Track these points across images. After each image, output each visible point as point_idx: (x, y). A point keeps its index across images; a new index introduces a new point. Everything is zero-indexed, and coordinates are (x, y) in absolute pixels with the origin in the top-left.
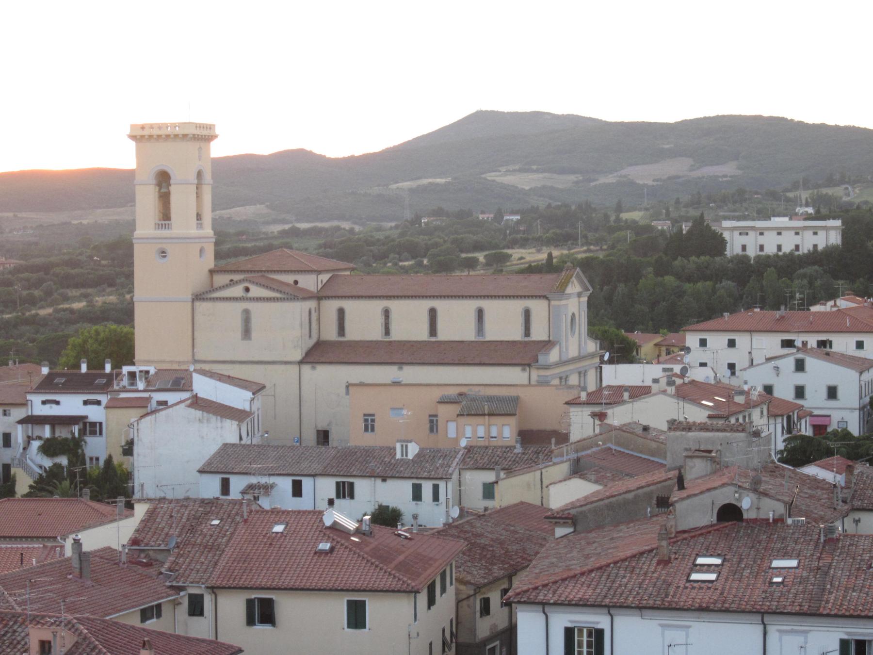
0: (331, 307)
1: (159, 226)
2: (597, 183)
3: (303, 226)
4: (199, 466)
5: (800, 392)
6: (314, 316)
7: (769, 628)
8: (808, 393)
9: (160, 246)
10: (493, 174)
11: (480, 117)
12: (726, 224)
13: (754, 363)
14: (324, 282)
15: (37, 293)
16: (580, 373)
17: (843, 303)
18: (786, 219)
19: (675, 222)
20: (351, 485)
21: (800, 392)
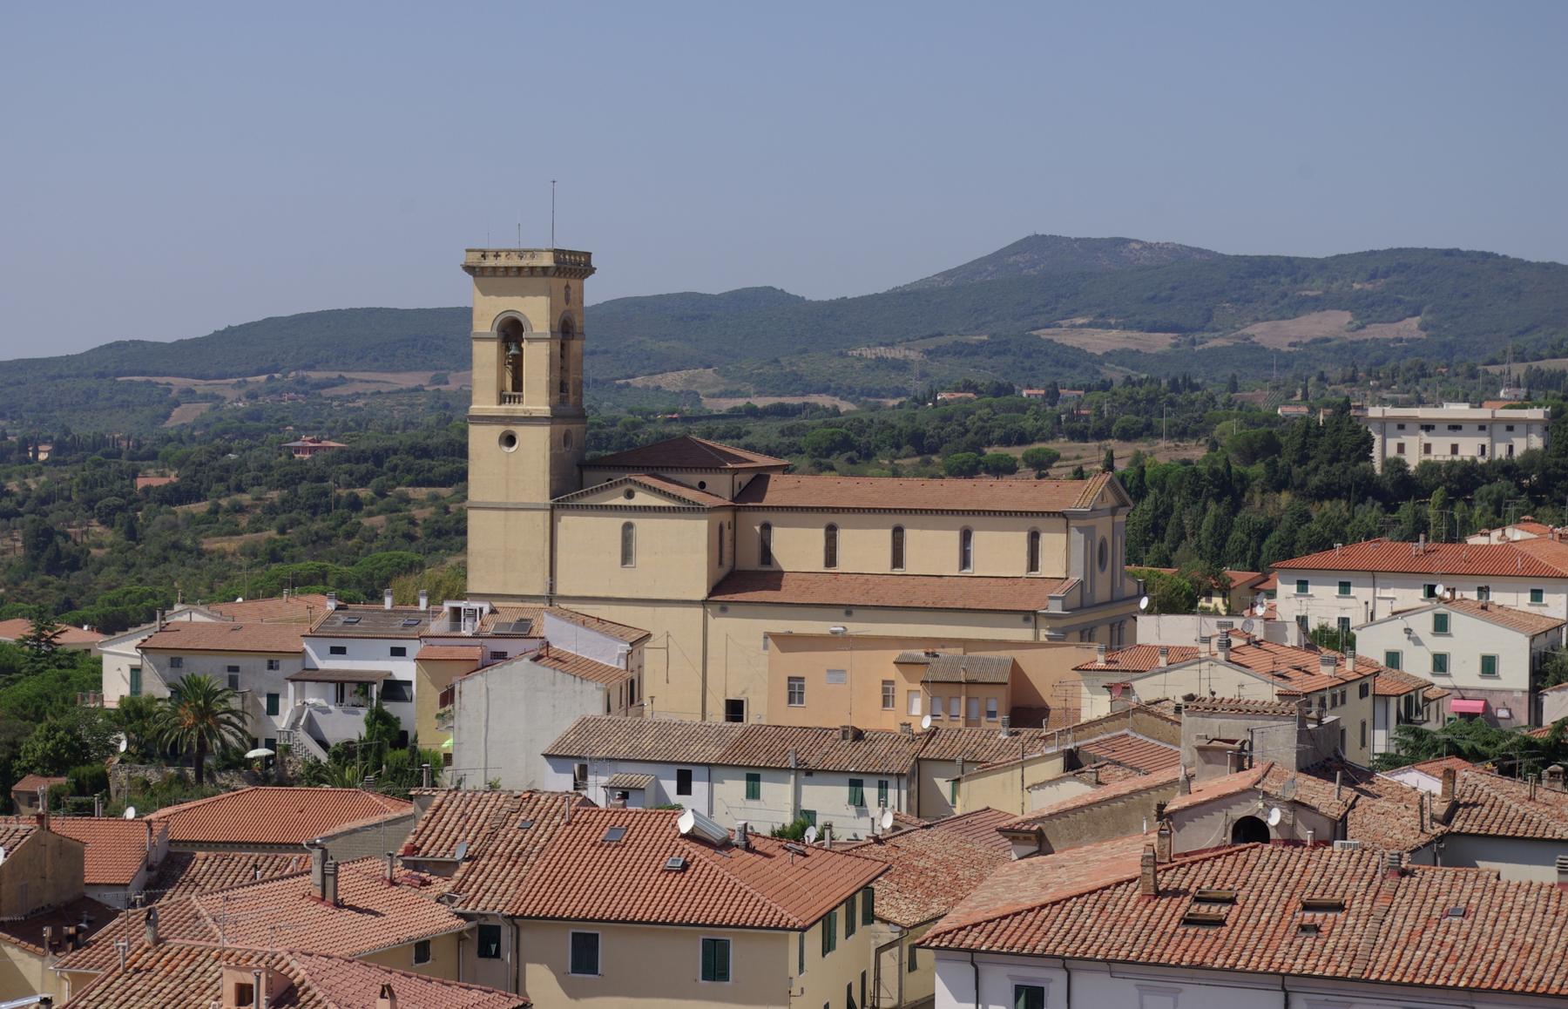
2: (1206, 346)
3: (761, 402)
4: (545, 748)
5: (1440, 664)
6: (727, 534)
7: (1293, 997)
8: (1453, 666)
10: (1050, 331)
11: (1036, 244)
12: (1375, 412)
13: (1378, 617)
14: (744, 484)
15: (364, 493)
16: (1112, 626)
17: (1515, 534)
18: (1466, 406)
19: (1313, 410)
21: (1440, 664)
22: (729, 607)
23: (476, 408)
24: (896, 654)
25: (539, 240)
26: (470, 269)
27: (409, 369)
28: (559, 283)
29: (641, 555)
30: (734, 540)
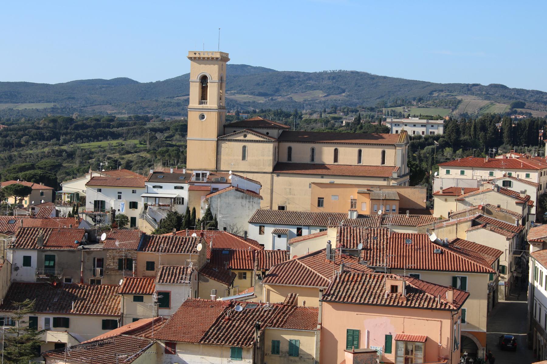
0: (285, 145)
1: (201, 103)
9: (201, 113)
20: (504, 185)
22: (280, 175)
23: (191, 105)
24: (357, 190)
25: (212, 48)
26: (190, 58)
27: (6, 102)
28: (221, 63)
29: (249, 158)
30: (278, 152)
